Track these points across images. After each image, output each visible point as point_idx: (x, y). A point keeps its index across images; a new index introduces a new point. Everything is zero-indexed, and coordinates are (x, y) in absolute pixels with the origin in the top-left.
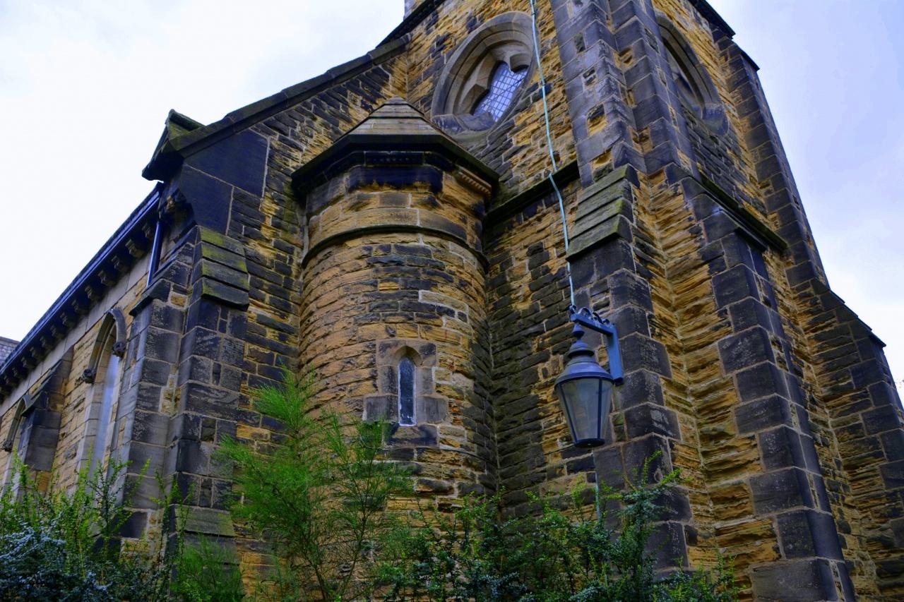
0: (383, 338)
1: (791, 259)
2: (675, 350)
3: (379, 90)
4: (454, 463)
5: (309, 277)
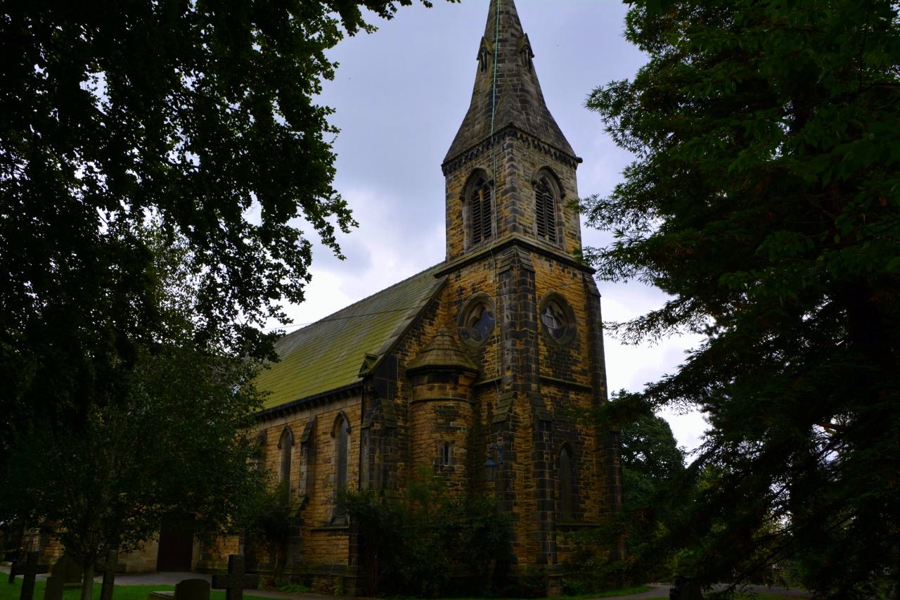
0: (439, 438)
1: (593, 395)
2: (521, 452)
3: (436, 311)
4: (460, 477)
5: (414, 409)
